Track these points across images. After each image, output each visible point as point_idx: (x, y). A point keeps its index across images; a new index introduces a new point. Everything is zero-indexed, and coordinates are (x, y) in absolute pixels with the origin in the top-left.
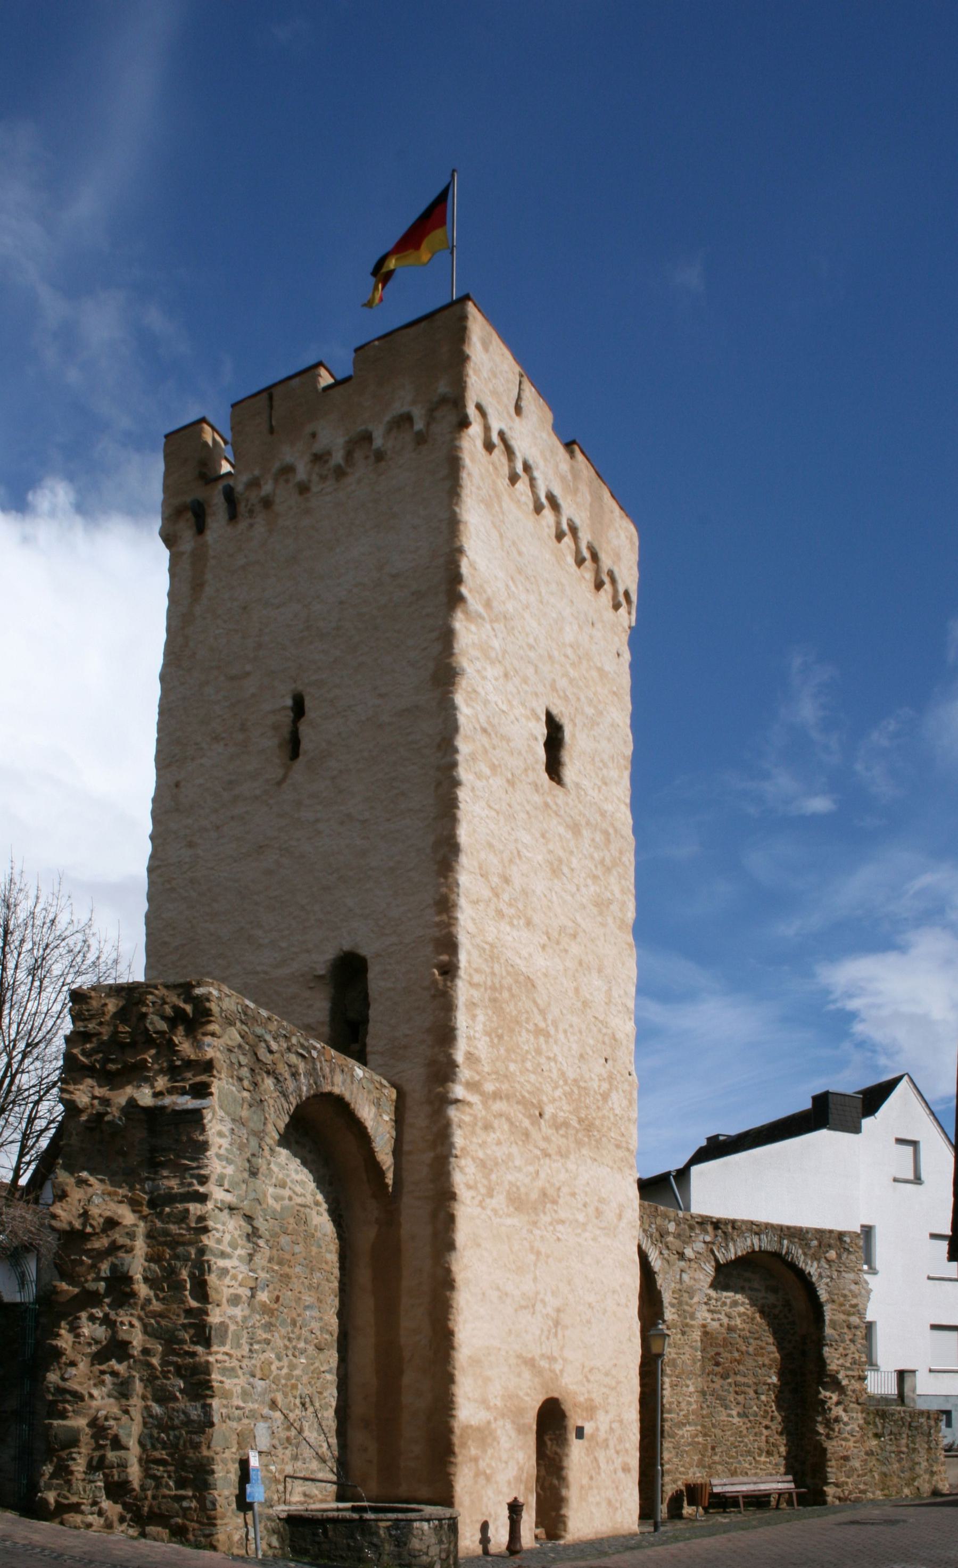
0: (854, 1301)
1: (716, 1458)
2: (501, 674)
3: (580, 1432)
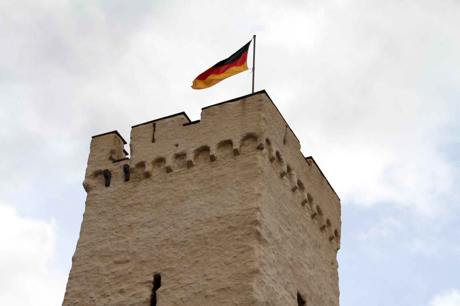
2: (276, 272)
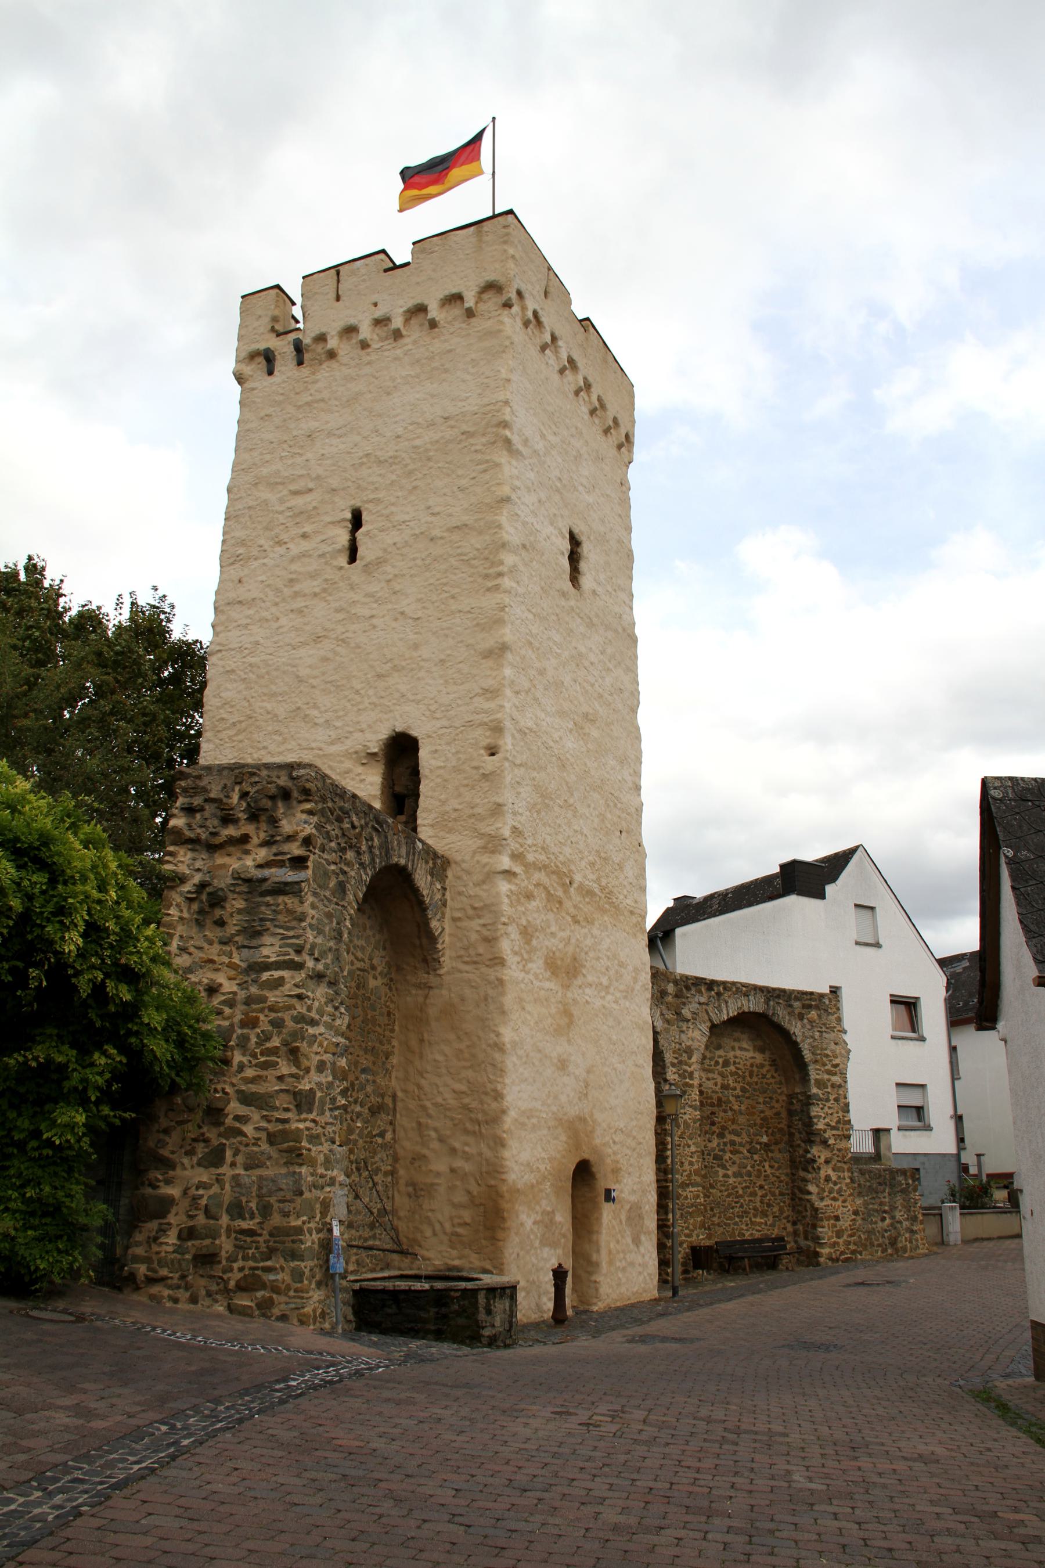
0: (836, 1061)
1: (716, 1220)
3: (608, 1196)
